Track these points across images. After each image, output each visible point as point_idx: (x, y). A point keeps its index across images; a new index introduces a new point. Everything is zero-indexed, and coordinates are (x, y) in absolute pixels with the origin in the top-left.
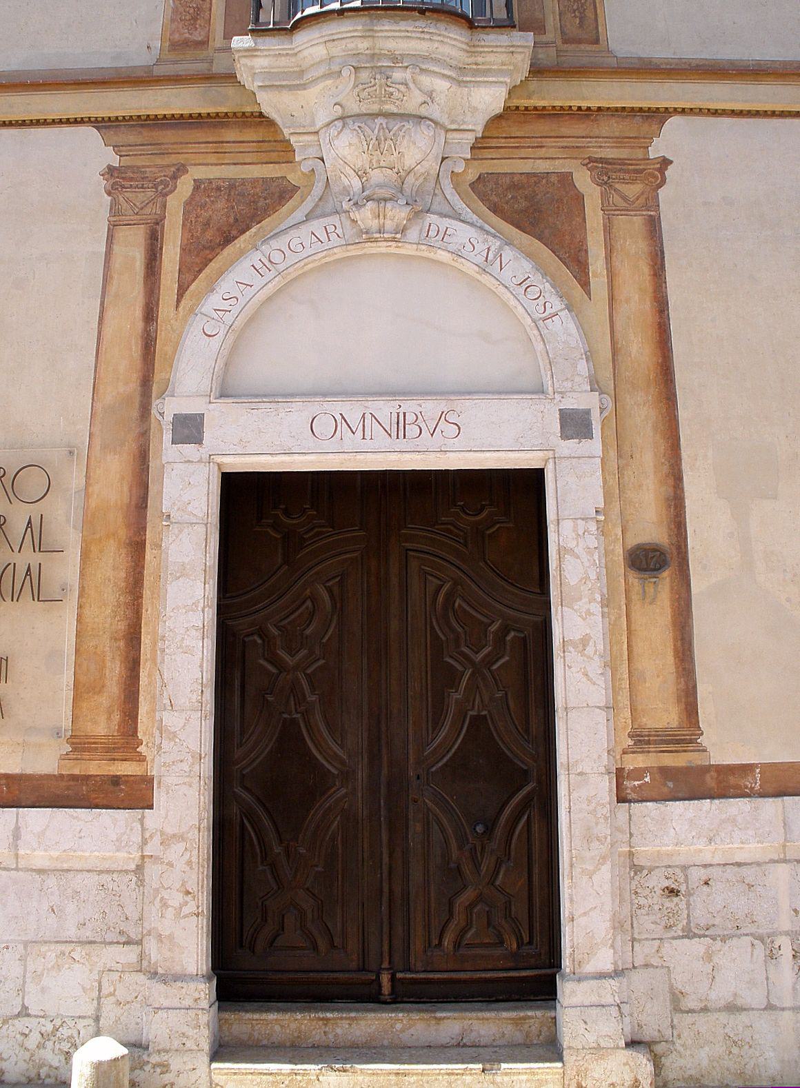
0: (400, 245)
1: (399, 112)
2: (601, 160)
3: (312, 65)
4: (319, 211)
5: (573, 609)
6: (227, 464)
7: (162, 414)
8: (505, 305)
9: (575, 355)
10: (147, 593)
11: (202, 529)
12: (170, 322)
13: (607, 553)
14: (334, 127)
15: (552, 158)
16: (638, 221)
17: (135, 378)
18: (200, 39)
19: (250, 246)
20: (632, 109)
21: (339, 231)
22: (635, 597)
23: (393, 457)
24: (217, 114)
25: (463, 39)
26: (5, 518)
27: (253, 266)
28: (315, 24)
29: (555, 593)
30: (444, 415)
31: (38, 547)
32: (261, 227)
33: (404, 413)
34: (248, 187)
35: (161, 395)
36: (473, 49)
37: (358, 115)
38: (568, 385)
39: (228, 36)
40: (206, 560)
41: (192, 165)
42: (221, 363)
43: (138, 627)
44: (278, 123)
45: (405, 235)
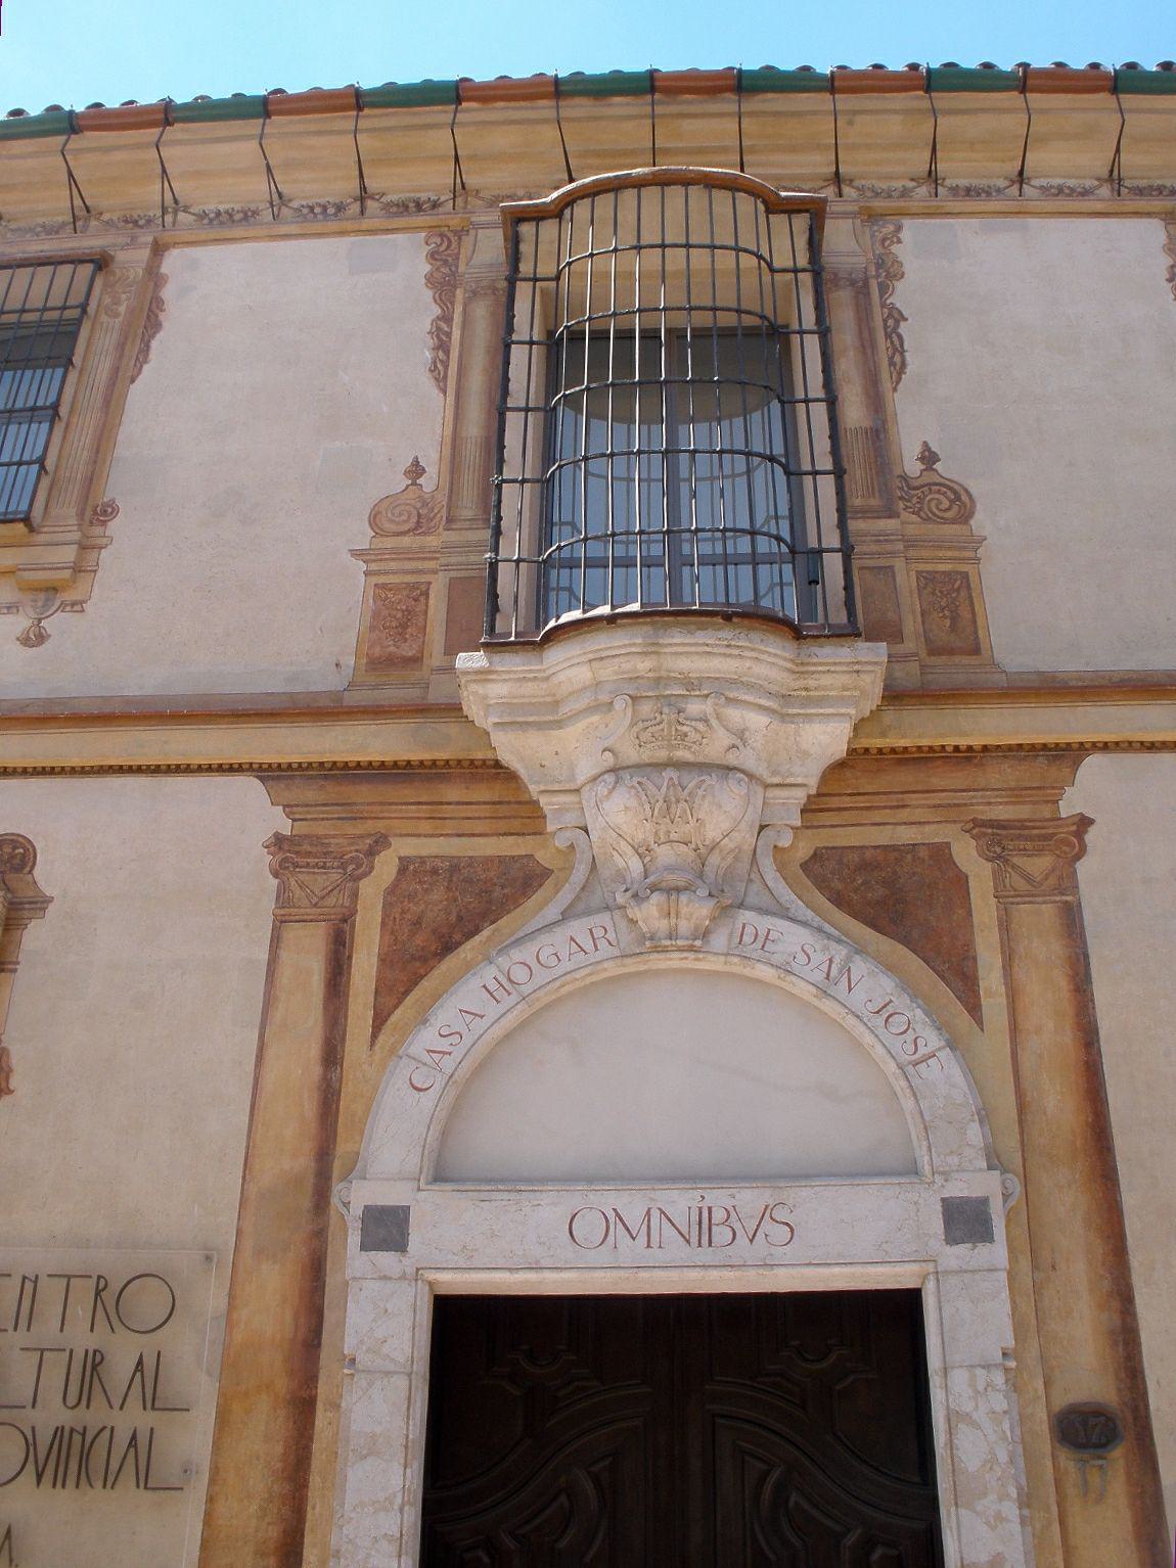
0: (701, 956)
1: (698, 760)
2: (991, 824)
3: (570, 694)
4: (581, 906)
5: (975, 1512)
6: (442, 1283)
7: (346, 1205)
8: (857, 1045)
9: (964, 1115)
10: (315, 1480)
11: (401, 1383)
12: (361, 1066)
13: (1023, 1419)
14: (603, 783)
15: (920, 823)
16: (1048, 912)
17: (308, 1147)
18: (410, 654)
19: (480, 957)
20: (1032, 747)
21: (611, 936)
22: (1071, 1491)
23: (694, 1274)
24: (434, 761)
25: (787, 655)
26: (102, 1355)
27: (484, 986)
28: (574, 636)
29: (944, 1486)
30: (768, 1211)
31: (152, 1402)
32: (496, 930)
33: (710, 1209)
34: (479, 869)
35: (346, 1176)
36: (801, 669)
37: (638, 766)
38: (954, 1160)
39: (451, 651)
40: (408, 1429)
41: (396, 835)
42: (434, 1133)
43: (299, 1535)
44: (522, 777)
45: (708, 942)
